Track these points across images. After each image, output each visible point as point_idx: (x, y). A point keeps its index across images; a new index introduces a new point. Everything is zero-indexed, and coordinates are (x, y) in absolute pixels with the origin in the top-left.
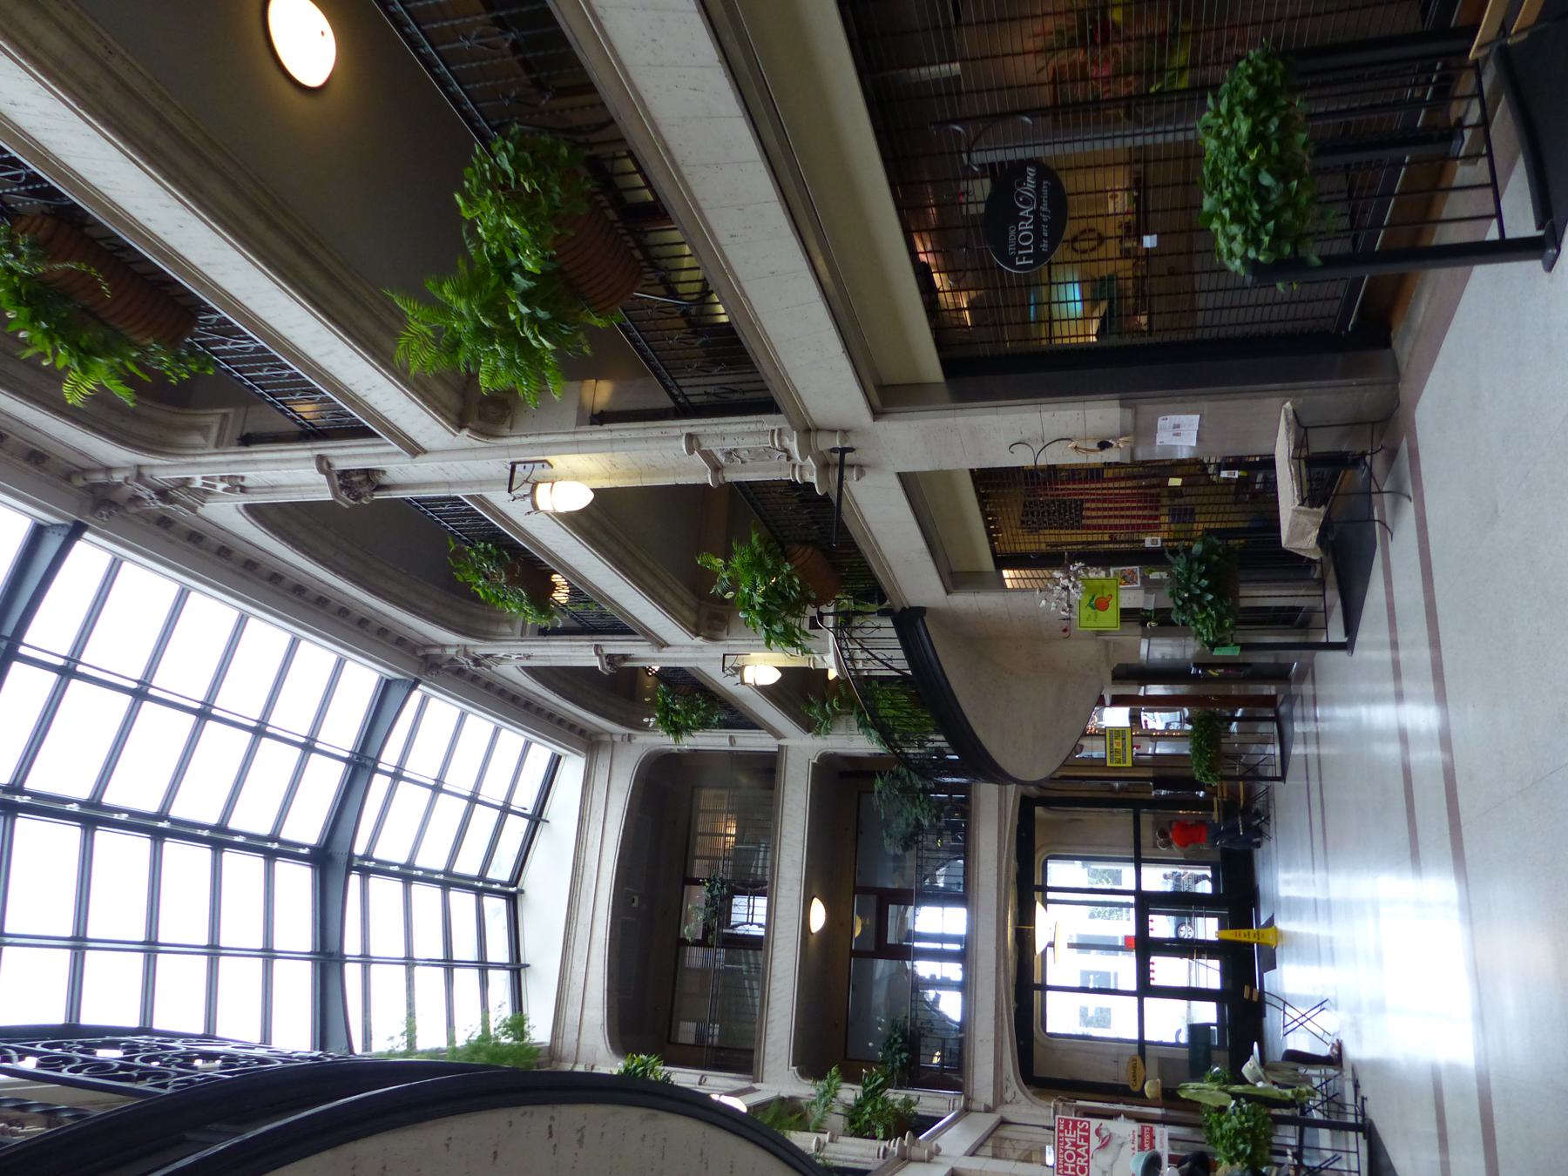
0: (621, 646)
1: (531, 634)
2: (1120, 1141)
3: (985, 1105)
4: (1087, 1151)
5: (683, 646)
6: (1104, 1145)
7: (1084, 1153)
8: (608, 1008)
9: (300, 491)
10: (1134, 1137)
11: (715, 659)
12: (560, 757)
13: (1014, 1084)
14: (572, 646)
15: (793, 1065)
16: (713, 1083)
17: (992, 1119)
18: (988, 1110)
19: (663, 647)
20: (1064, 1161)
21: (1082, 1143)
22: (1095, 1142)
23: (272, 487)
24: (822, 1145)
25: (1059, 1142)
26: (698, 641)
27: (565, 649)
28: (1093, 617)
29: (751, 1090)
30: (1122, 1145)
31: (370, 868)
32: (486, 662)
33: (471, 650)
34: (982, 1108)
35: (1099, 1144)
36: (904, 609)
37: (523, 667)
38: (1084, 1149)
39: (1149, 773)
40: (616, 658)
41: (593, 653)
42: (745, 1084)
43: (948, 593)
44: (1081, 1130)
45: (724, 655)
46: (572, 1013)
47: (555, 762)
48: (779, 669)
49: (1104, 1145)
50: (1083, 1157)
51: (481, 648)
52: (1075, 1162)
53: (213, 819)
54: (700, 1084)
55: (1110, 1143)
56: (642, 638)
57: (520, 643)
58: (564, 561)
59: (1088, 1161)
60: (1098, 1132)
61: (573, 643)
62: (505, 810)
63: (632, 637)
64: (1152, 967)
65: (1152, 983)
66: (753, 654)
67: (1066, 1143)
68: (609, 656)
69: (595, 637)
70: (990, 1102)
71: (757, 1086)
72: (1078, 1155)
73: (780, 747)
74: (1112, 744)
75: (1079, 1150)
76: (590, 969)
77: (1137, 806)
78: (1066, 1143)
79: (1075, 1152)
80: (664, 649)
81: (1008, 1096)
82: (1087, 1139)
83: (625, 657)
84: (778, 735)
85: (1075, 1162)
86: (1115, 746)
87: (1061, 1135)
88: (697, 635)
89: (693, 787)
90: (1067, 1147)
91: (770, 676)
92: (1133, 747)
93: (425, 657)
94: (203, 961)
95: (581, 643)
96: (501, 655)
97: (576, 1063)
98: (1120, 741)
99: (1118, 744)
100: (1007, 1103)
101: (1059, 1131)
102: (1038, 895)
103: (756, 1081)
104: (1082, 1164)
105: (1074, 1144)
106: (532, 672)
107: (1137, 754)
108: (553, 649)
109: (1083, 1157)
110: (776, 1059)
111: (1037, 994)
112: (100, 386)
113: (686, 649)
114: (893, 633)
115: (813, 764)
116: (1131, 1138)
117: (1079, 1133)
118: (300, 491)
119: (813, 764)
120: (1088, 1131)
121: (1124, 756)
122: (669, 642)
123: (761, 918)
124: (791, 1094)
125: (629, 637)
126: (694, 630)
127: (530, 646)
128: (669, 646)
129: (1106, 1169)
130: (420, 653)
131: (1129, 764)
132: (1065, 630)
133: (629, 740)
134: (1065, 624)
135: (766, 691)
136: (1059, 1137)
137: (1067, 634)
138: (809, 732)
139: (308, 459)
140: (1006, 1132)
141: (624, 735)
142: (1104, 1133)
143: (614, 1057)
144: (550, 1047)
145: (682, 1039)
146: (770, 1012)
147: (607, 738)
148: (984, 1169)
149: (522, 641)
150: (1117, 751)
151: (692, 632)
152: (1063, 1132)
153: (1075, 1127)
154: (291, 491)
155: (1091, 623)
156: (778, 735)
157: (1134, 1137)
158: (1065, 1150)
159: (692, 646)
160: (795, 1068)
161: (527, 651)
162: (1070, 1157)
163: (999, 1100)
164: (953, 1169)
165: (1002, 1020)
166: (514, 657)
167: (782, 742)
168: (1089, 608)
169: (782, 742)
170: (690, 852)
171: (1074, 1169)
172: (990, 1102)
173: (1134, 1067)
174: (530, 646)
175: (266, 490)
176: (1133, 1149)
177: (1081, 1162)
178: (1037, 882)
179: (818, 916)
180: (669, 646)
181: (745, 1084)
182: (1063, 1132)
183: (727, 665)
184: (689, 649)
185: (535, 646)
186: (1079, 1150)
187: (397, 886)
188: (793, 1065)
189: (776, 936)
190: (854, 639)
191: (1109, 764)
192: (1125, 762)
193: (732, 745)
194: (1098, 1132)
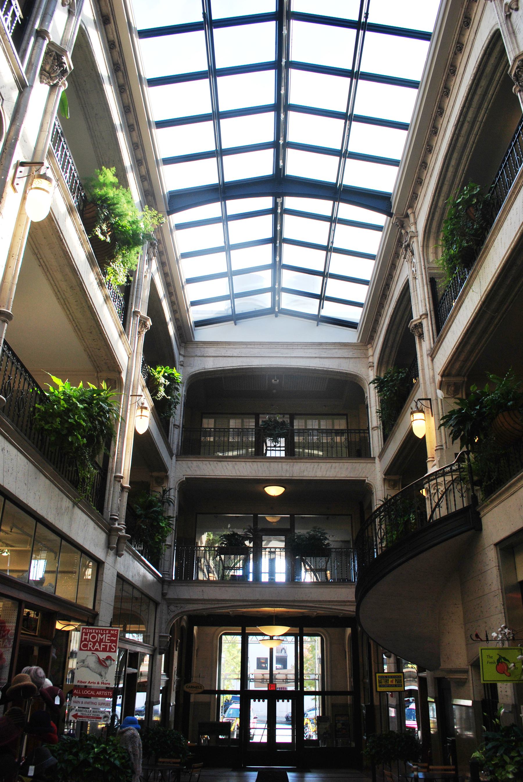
0: (428, 330)
1: (430, 273)
2: (103, 673)
3: (166, 594)
4: (97, 650)
5: (433, 370)
6: (101, 663)
7: (95, 647)
8: (214, 371)
9: (514, 49)
10: (106, 684)
11: (426, 394)
12: (356, 328)
13: (180, 611)
14: (425, 300)
15: (186, 478)
16: (175, 432)
17: (158, 598)
18: (164, 595)
19: (431, 356)
20: (91, 633)
21: (102, 646)
22: (103, 655)
23: (514, 32)
24: (118, 479)
25: (103, 630)
26: (438, 378)
27: (422, 296)
28: (491, 660)
29: (171, 454)
30: (101, 675)
31: (279, 170)
32: (409, 253)
33: (415, 239)
34: (165, 591)
35: (101, 658)
36: (479, 513)
37: (408, 280)
38: (98, 647)
39: (376, 702)
40: (420, 330)
41: (421, 313)
42: (175, 451)
43: (496, 545)
44: (110, 646)
45: (430, 399)
46: (211, 351)
47: (351, 325)
48: (424, 437)
49: (101, 663)
50: (93, 647)
51: (417, 245)
52: (90, 641)
53: (293, 100)
54: (174, 425)
55: (102, 666)
56: (436, 340)
57: (423, 267)
58: (486, 256)
59: (90, 650)
60: (109, 658)
61: (427, 300)
62: (321, 297)
63: (435, 334)
64: (286, 701)
65: (252, 700)
66: (433, 419)
67: (102, 635)
68: (421, 324)
69: (433, 313)
70: (168, 596)
71: (174, 457)
72: (94, 643)
73: (374, 458)
74: (391, 677)
75: (97, 644)
76: (235, 358)
77: (355, 693)
78: (102, 635)
79: (97, 641)
80: (430, 358)
81: (172, 608)
82: (104, 650)
83: (421, 336)
84: (381, 455)
85: (90, 641)
86: (390, 680)
87: (107, 632)
88: (442, 376)
89: (346, 415)
90: (99, 635)
91: (419, 433)
92: (391, 692)
93: (407, 216)
94: (208, 110)
95: (428, 305)
96: (414, 260)
97: (184, 356)
98: (394, 683)
99: (392, 681)
100: (168, 607)
101: (110, 630)
102: (296, 630)
103: (177, 456)
104: (89, 646)
105: (101, 640)
106: (406, 288)
107: (387, 695)
108: (421, 288)
109: (93, 647)
110: (189, 467)
111: (239, 630)
112: (51, 219)
113: (431, 372)
114: (459, 507)
115: (365, 480)
116: (105, 682)
117: (108, 644)
118: (514, 49)
119: (365, 480)
120: (110, 651)
121: (384, 686)
122: (435, 360)
123: (273, 454)
124: (170, 477)
125: (435, 331)
126: (446, 373)
127: (422, 274)
128: (432, 360)
129: (86, 663)
130: (409, 211)
131: (379, 689)
132: (477, 636)
133: (370, 367)
134: (483, 637)
135: (411, 433)
136: (106, 630)
137: (474, 637)
138: (385, 475)
139: (426, 309)
140: (152, 606)
141: (373, 363)
142: (108, 662)
143: (188, 377)
144: (192, 341)
145: (205, 421)
146: (215, 462)
147: (370, 352)
148: (104, 583)
149: (425, 268)
150: (387, 681)
151: (444, 371)
152: (109, 633)
153: (112, 641)
154: (513, 43)
155: (485, 659)
156: (381, 455)
157: (106, 684)
158: (98, 634)
159: (434, 376)
160: (184, 479)
161: (419, 277)
162: (93, 637)
163: (170, 602)
164: (103, 563)
165: (215, 604)
166: (414, 269)
167: (377, 460)
168: (498, 657)
169: (377, 460)
170: (309, 417)
171: (86, 639)
172: (168, 596)
173: (196, 687)
174: (422, 274)
175: (511, 29)
176: (98, 683)
177: (90, 646)
178: (306, 630)
179: (274, 491)
180: (432, 360)
181: (175, 451)
182: (109, 633)
183: (424, 402)
184: (431, 374)
185: (422, 278)
186: (97, 644)
187: (269, 234)
188: (186, 478)
189: (259, 463)
190: (452, 484)
191: (378, 675)
192: (380, 686)
193: (372, 429)
194: (109, 658)
